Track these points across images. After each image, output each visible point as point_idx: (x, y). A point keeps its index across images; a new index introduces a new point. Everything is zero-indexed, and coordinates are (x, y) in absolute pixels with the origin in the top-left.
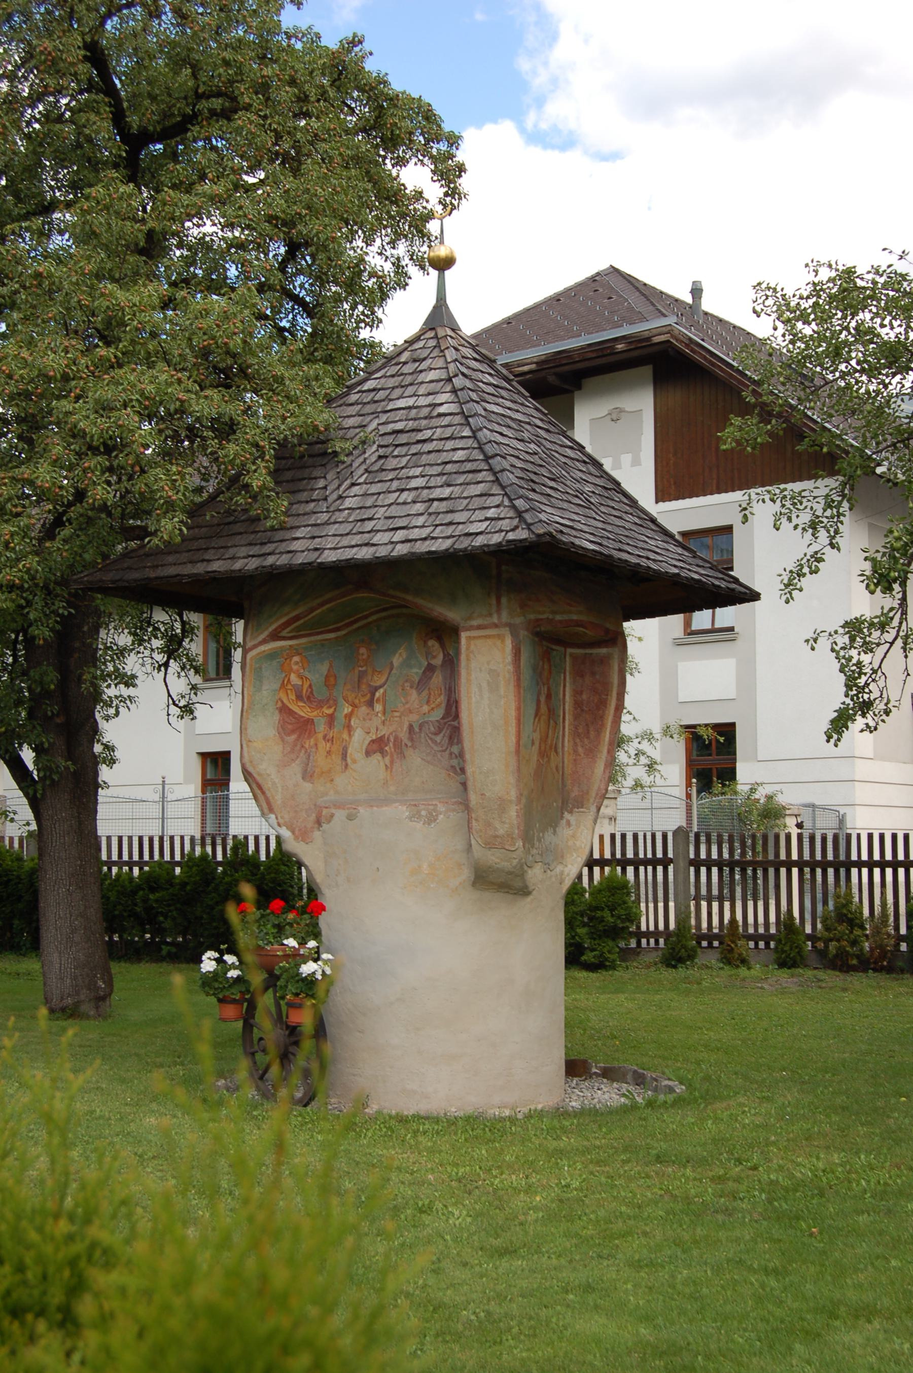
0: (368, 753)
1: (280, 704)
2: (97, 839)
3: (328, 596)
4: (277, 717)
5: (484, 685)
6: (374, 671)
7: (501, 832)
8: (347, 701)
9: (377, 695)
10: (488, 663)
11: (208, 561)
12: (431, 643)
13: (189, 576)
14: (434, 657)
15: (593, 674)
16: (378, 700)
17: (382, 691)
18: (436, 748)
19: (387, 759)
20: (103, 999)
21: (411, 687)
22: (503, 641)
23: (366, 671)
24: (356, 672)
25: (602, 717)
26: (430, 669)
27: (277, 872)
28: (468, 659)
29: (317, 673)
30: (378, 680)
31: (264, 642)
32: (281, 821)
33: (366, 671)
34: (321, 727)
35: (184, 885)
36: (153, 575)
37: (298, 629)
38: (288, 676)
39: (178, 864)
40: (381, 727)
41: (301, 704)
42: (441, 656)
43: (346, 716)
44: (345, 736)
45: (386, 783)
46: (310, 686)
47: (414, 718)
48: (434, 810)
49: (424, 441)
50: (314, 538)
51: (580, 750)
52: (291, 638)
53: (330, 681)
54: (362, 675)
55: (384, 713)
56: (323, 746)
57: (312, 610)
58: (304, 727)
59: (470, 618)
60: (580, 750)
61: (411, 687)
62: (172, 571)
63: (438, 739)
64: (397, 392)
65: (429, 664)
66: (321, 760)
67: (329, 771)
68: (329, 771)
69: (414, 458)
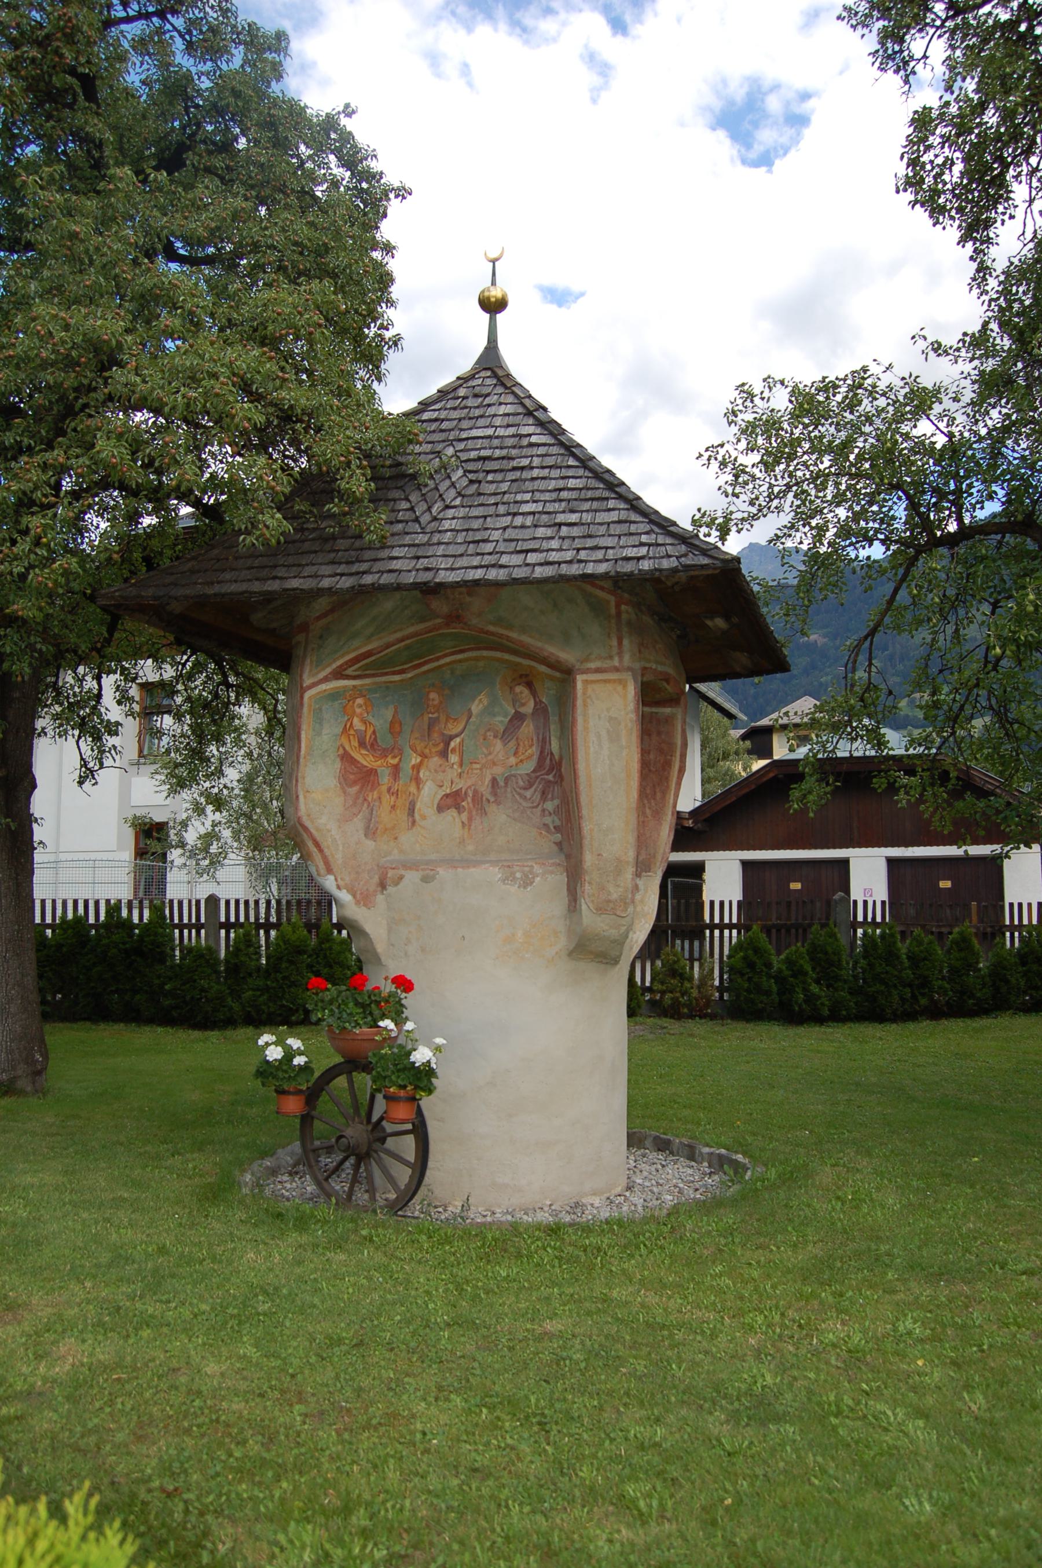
0: (440, 809)
1: (341, 751)
4: (338, 765)
5: (604, 733)
6: (448, 718)
7: (614, 896)
8: (415, 751)
9: (452, 744)
10: (608, 710)
11: (281, 578)
12: (518, 689)
13: (261, 593)
14: (523, 705)
15: (659, 733)
16: (453, 750)
17: (458, 740)
18: (524, 804)
19: (464, 816)
20: (39, 1073)
21: (495, 737)
22: (625, 687)
23: (438, 718)
24: (426, 718)
25: (667, 779)
26: (518, 718)
27: (156, 934)
28: (585, 705)
29: (382, 718)
30: (453, 729)
31: (325, 680)
32: (340, 882)
33: (438, 718)
34: (385, 779)
35: (59, 946)
36: (210, 591)
37: (367, 667)
38: (350, 720)
39: (49, 926)
40: (457, 780)
41: (364, 752)
42: (532, 703)
43: (413, 767)
44: (413, 789)
45: (462, 842)
46: (374, 732)
47: (498, 770)
48: (531, 872)
49: (522, 468)
50: (418, 558)
51: (648, 811)
52: (354, 678)
53: (395, 727)
55: (461, 765)
56: (387, 800)
58: (367, 778)
59: (587, 659)
60: (648, 811)
61: (495, 737)
62: (233, 588)
63: (528, 794)
64: (465, 424)
65: (517, 712)
66: (384, 815)
67: (393, 828)
68: (393, 828)
69: (516, 484)
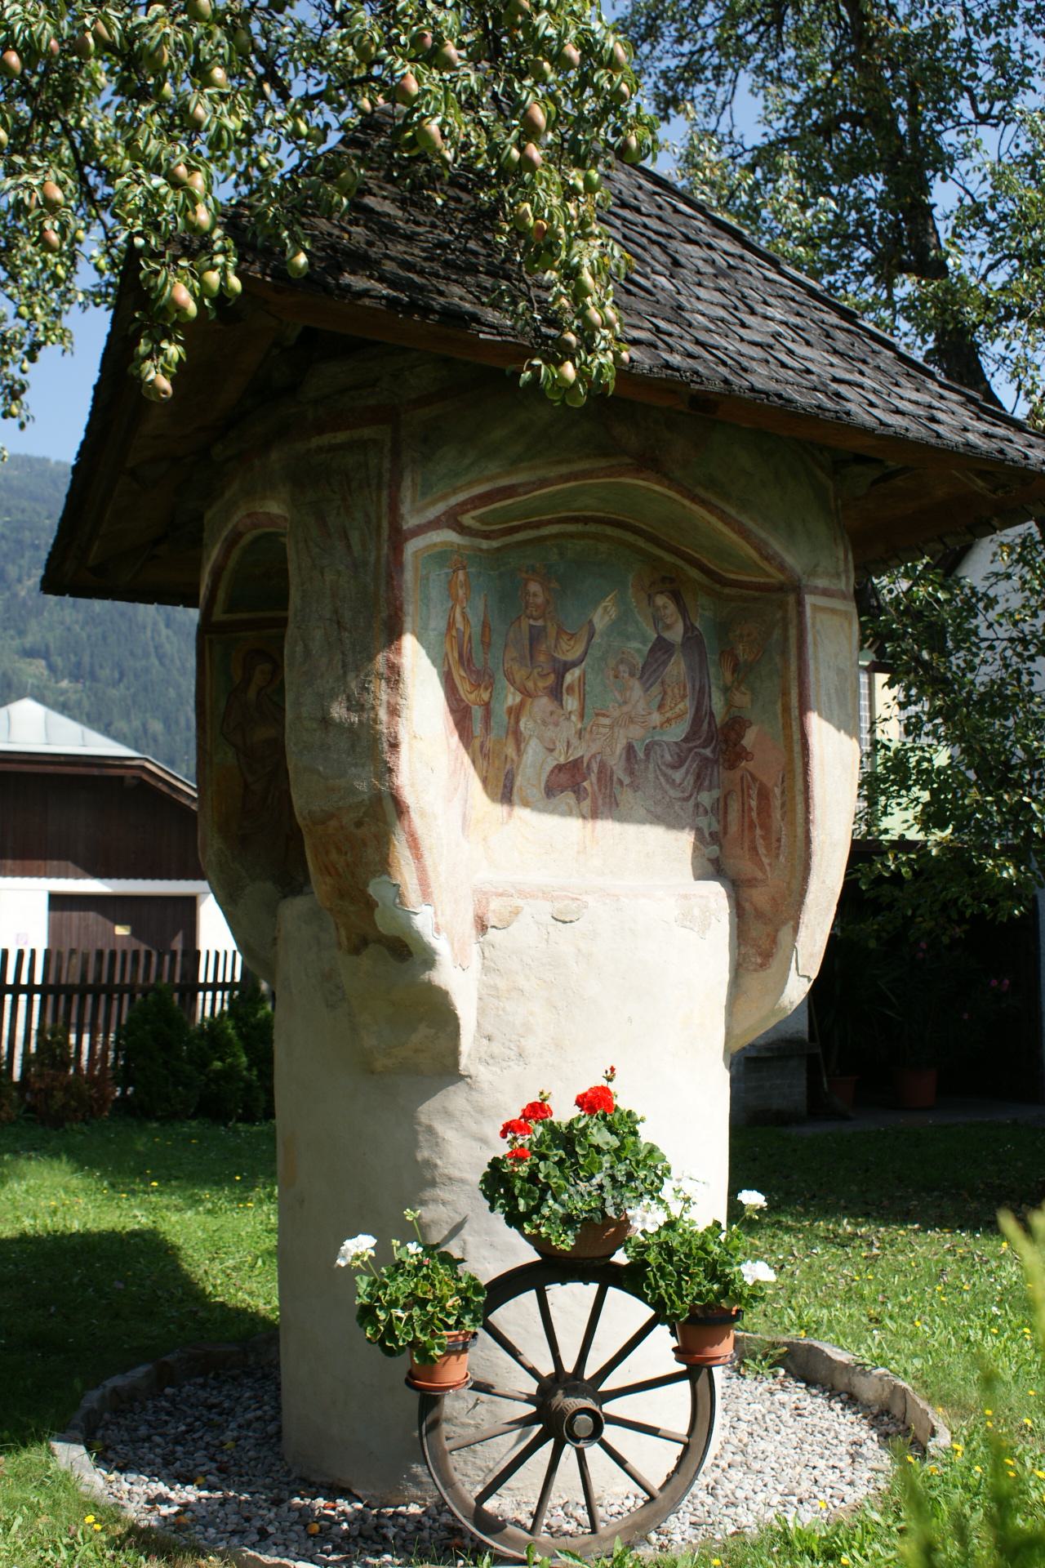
2: (199, 953)
3: (584, 465)
6: (560, 631)
8: (513, 683)
9: (569, 678)
14: (668, 627)
16: (570, 689)
17: (577, 672)
18: (672, 793)
21: (632, 675)
26: (662, 648)
43: (510, 710)
44: (510, 751)
47: (636, 732)
54: (536, 637)
55: (582, 716)
57: (543, 483)
61: (632, 675)
63: (678, 776)
65: (660, 638)
